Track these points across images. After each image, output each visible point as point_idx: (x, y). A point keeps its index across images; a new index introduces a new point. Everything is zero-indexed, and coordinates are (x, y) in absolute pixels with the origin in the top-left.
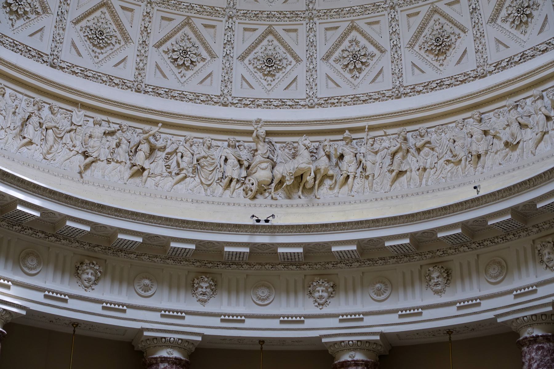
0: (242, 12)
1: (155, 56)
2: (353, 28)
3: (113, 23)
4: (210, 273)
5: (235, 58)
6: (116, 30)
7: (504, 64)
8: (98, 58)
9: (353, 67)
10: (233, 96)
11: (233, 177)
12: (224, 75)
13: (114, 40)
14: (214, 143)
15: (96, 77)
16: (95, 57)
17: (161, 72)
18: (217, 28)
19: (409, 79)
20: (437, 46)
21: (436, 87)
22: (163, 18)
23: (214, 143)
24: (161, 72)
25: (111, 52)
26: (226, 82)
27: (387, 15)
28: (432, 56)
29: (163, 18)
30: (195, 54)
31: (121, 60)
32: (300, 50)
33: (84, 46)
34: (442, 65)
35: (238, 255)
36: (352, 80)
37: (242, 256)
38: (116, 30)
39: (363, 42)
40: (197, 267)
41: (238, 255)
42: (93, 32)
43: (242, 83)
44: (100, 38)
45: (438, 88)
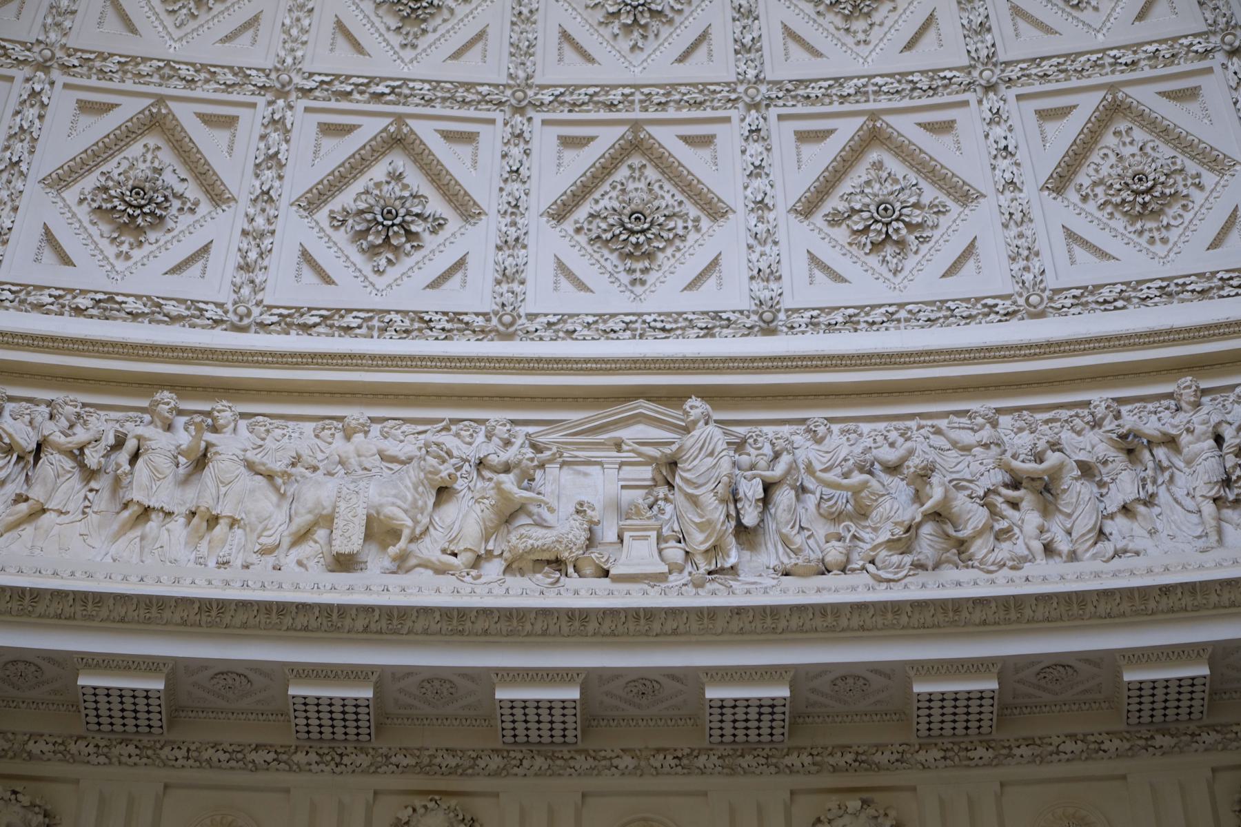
1: (799, 238)
2: (398, 141)
7: (877, 316)
9: (380, 241)
12: (504, 229)
18: (242, 126)
19: (802, 290)
20: (122, 197)
21: (359, 327)
22: (1044, 115)
24: (825, 268)
27: (500, 122)
28: (106, 228)
29: (1044, 115)
32: (235, 173)
34: (379, 272)
35: (1160, 692)
36: (373, 277)
37: (1160, 695)
39: (415, 180)
41: (1160, 692)
43: (810, 270)
45: (321, 329)
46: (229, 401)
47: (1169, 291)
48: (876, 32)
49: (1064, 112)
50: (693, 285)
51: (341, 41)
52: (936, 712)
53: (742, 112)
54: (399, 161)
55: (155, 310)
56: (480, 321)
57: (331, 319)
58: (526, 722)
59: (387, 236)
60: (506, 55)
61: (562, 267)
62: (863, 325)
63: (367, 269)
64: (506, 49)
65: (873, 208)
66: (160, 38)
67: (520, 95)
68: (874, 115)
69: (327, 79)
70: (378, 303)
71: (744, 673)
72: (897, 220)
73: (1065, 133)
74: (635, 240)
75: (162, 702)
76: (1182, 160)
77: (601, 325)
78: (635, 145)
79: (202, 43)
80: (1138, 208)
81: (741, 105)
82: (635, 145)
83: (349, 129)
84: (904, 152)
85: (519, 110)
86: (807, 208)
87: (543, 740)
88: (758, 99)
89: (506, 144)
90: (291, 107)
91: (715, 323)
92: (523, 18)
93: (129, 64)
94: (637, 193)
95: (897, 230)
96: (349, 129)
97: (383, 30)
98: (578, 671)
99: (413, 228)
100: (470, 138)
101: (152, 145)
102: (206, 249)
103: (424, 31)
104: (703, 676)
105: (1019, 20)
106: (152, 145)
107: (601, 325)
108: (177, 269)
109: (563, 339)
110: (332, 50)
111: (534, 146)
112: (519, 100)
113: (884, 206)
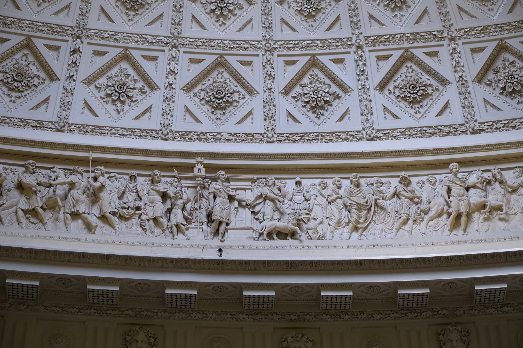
0: (372, 38)
1: (284, 104)
3: (423, 74)
4: (151, 325)
5: (470, 82)
6: (429, 78)
7: (88, 128)
8: (420, 113)
10: (479, 121)
11: (461, 211)
13: (236, 96)
14: (383, 180)
15: (319, 137)
16: (217, 119)
17: (376, 20)
22: (379, 58)
23: (383, 180)
24: (376, 20)
25: (431, 101)
26: (270, 117)
27: (261, 55)
29: (379, 58)
30: (328, 93)
31: (347, 114)
33: (202, 112)
36: (316, 120)
38: (429, 78)
40: (396, 319)
42: (210, 94)
44: (415, 92)
46: (355, 172)
47: (423, 132)
48: (137, 18)
50: (240, 122)
51: (102, 16)
52: (329, 302)
53: (263, 52)
54: (124, 65)
55: (24, 123)
56: (154, 133)
58: (23, 291)
59: (119, 97)
60: (261, 28)
61: (290, 115)
62: (82, 132)
63: (313, 116)
64: (171, 21)
65: (116, 86)
66: (29, 12)
67: (175, 41)
68: (314, 55)
69: (375, 38)
70: (114, 124)
72: (124, 93)
74: (220, 102)
75: (274, 299)
78: (221, 63)
79: (47, 16)
80: (412, 99)
81: (170, 46)
82: (221, 63)
85: (175, 46)
87: (114, 303)
88: (177, 44)
89: (169, 60)
90: (82, 42)
91: (145, 133)
92: (178, 9)
93: (113, 36)
95: (123, 96)
97: (120, 13)
98: (274, 284)
99: (130, 94)
100: (155, 59)
101: (409, 66)
103: (137, 14)
104: (320, 287)
105: (372, 20)
106: (409, 66)
108: (35, 108)
109: (204, 142)
110: (371, 26)
111: (275, 65)
112: (175, 43)
113: (122, 85)
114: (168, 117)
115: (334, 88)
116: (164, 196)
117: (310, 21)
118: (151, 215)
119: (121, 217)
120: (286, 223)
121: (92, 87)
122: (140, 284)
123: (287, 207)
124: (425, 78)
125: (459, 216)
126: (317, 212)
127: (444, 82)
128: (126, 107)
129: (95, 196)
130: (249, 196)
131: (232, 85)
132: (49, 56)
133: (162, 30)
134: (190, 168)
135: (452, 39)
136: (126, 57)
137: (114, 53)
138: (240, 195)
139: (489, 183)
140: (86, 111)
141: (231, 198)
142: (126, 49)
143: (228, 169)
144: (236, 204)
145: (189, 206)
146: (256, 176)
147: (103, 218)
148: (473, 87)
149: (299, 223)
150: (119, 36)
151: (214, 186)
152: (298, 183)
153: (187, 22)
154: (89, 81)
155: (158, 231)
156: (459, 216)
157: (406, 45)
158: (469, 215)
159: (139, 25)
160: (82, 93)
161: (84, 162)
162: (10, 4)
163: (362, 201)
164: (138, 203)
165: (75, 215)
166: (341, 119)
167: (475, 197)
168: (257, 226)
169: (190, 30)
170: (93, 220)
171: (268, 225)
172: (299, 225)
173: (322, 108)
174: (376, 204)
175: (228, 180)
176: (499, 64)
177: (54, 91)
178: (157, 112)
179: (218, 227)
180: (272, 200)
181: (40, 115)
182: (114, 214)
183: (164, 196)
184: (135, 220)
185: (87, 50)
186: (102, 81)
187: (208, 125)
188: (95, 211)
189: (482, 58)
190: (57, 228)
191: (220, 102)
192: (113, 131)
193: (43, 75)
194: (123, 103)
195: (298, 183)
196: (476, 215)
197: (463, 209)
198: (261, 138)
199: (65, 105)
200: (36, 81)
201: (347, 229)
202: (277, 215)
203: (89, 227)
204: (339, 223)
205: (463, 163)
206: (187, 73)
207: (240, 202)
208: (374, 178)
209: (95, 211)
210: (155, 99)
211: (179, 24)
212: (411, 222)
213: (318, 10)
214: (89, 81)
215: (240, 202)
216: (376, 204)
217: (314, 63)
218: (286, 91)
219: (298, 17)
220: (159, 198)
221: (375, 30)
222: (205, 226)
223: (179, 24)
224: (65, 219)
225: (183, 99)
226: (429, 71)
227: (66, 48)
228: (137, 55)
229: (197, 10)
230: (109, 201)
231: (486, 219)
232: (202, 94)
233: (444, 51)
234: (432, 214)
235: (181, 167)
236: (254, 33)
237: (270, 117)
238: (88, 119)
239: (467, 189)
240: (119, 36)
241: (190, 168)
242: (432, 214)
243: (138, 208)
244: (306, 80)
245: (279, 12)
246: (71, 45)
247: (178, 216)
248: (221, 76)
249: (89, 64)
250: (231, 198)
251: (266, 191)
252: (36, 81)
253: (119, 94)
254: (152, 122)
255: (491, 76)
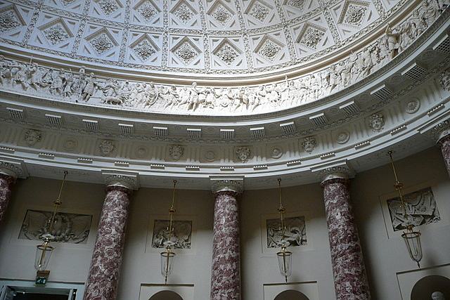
22: (174, 38)
26: (122, 56)
29: (46, 17)
32: (201, 47)
49: (257, 39)
54: (59, 24)
57: (39, 49)
71: (345, 102)
73: (257, 42)
74: (102, 47)
76: (228, 12)
77: (223, 72)
83: (50, 17)
84: (191, 43)
86: (132, 47)
92: (88, 4)
93: (55, 10)
94: (103, 37)
96: (50, 17)
102: (19, 33)
107: (223, 72)
114: (80, 49)
115: (153, 48)
116: (64, 80)
117: (147, 19)
118: (56, 87)
119: (41, 86)
120: (117, 98)
121: (42, 31)
122: (361, 96)
123: (119, 92)
124: (192, 49)
125: (193, 104)
126: (133, 96)
127: (200, 52)
128: (57, 42)
129: (30, 75)
130: (103, 85)
131: (108, 40)
132: (23, 14)
133: (79, 12)
134: (79, 70)
135: (206, 35)
136: (60, 21)
137: (55, 18)
138: (99, 84)
139: (209, 93)
140: (37, 41)
141: (95, 85)
142: (61, 17)
143: (95, 72)
144: (97, 88)
145: (74, 86)
146: (108, 78)
147: (32, 85)
148: (211, 55)
149: (123, 99)
150: (58, 11)
151: (87, 79)
152: (127, 83)
153: (91, 9)
154: (41, 28)
155: (58, 94)
156: (193, 104)
157: (186, 34)
158: (197, 105)
159: (69, 8)
160: (36, 32)
161: (28, 60)
162: (52, 1)
163: (153, 93)
164: (51, 81)
165: (18, 82)
166: (153, 61)
167: (201, 97)
168: (104, 98)
169: (92, 14)
170: (27, 85)
171: (109, 98)
172: (123, 101)
173: (146, 55)
174: (159, 96)
175: (95, 78)
176: (224, 48)
177: (23, 30)
178: (202, 62)
179: (86, 96)
180: (113, 88)
181: (13, 39)
182: (38, 84)
183: (64, 80)
184: (48, 88)
185: (42, 14)
186: (48, 29)
187: (93, 55)
188: (29, 81)
189: (216, 44)
190: (9, 86)
191: (102, 47)
192: (47, 51)
193: (19, 22)
194: (56, 40)
195: (127, 83)
196: (200, 105)
197: (195, 101)
198: (117, 64)
199: (27, 37)
200: (15, 24)
201: (144, 104)
202: (114, 95)
203: (24, 88)
204: (141, 101)
205: (199, 84)
206: (88, 32)
207: (98, 87)
208: (161, 85)
209: (29, 81)
210: (71, 41)
211: (87, 10)
212: (172, 105)
213: (151, 15)
214: (41, 28)
215: (98, 87)
216: (159, 96)
217: (146, 37)
218: (132, 47)
219: (142, 16)
220: (61, 80)
221: (174, 26)
222: (80, 95)
223: (87, 10)
224: (13, 83)
225: (84, 43)
226: (194, 46)
227: (31, 12)
228: (66, 21)
229: (97, 6)
230: (37, 77)
231: (204, 107)
232: (180, 53)
233: (201, 39)
234: (182, 102)
235: (73, 69)
236: (121, 20)
237: (122, 56)
238: (37, 44)
239: (199, 94)
240: (58, 11)
241: (79, 70)
242: (182, 102)
243: (50, 83)
244: (141, 43)
245: (93, 4)
246: (34, 11)
247: (68, 89)
248: (104, 36)
249: (42, 21)
250: (95, 85)
251: (111, 84)
252: (15, 24)
253: (55, 37)
254: (68, 50)
255: (219, 52)
